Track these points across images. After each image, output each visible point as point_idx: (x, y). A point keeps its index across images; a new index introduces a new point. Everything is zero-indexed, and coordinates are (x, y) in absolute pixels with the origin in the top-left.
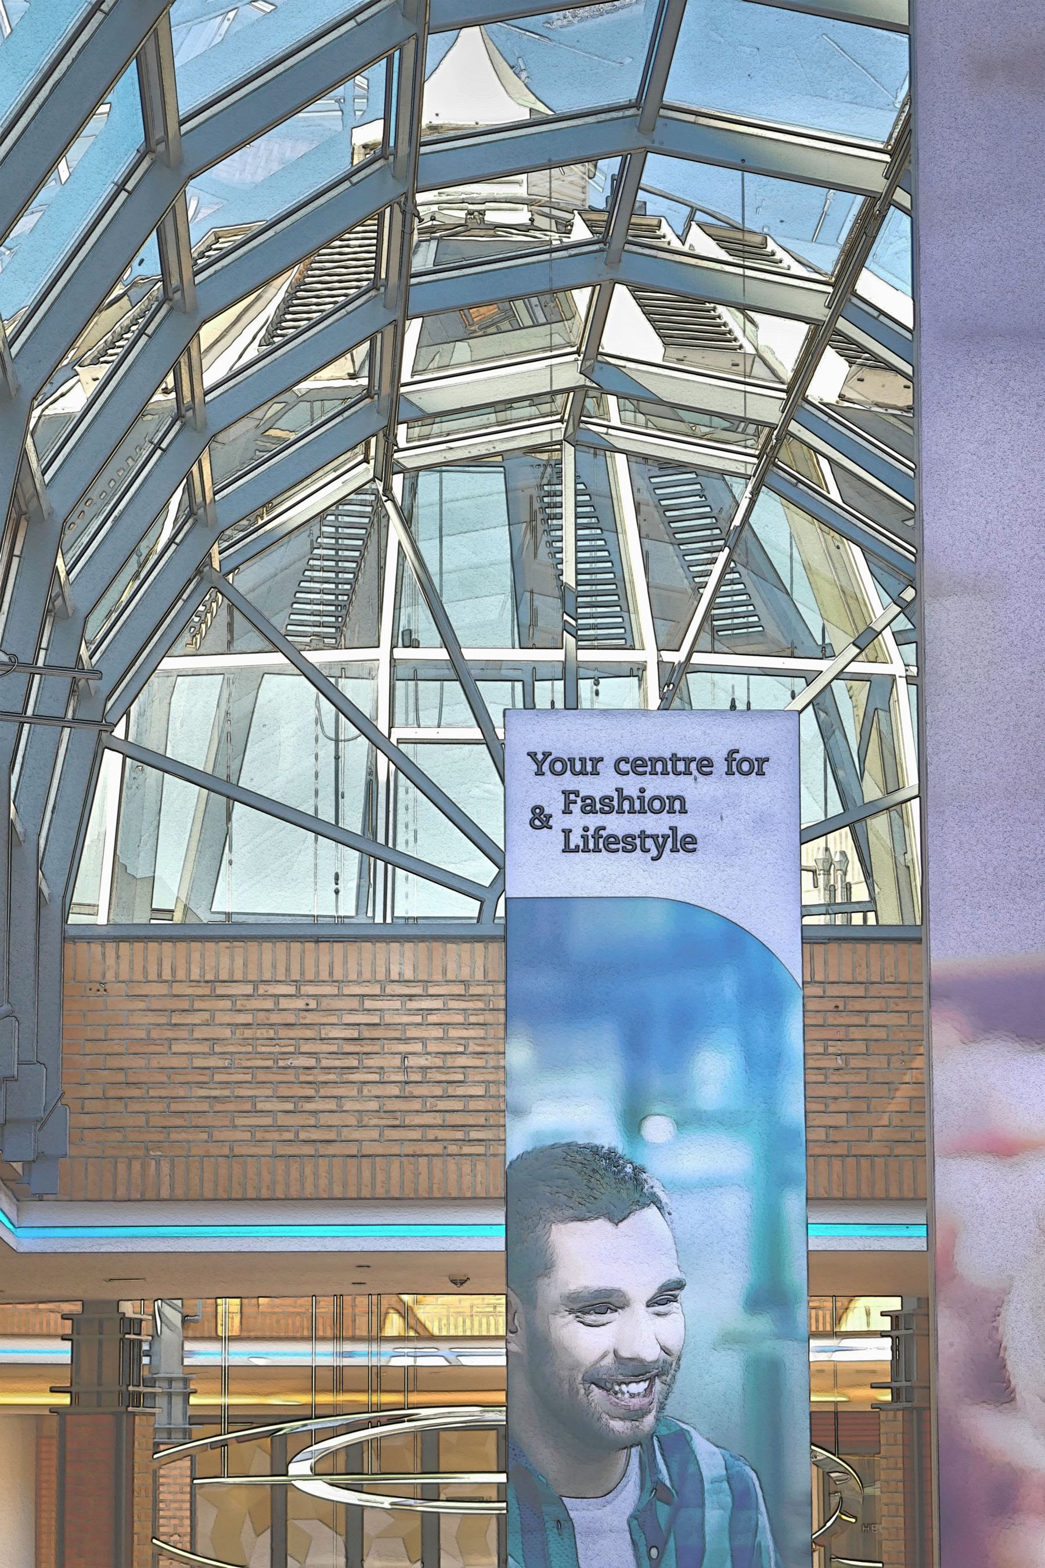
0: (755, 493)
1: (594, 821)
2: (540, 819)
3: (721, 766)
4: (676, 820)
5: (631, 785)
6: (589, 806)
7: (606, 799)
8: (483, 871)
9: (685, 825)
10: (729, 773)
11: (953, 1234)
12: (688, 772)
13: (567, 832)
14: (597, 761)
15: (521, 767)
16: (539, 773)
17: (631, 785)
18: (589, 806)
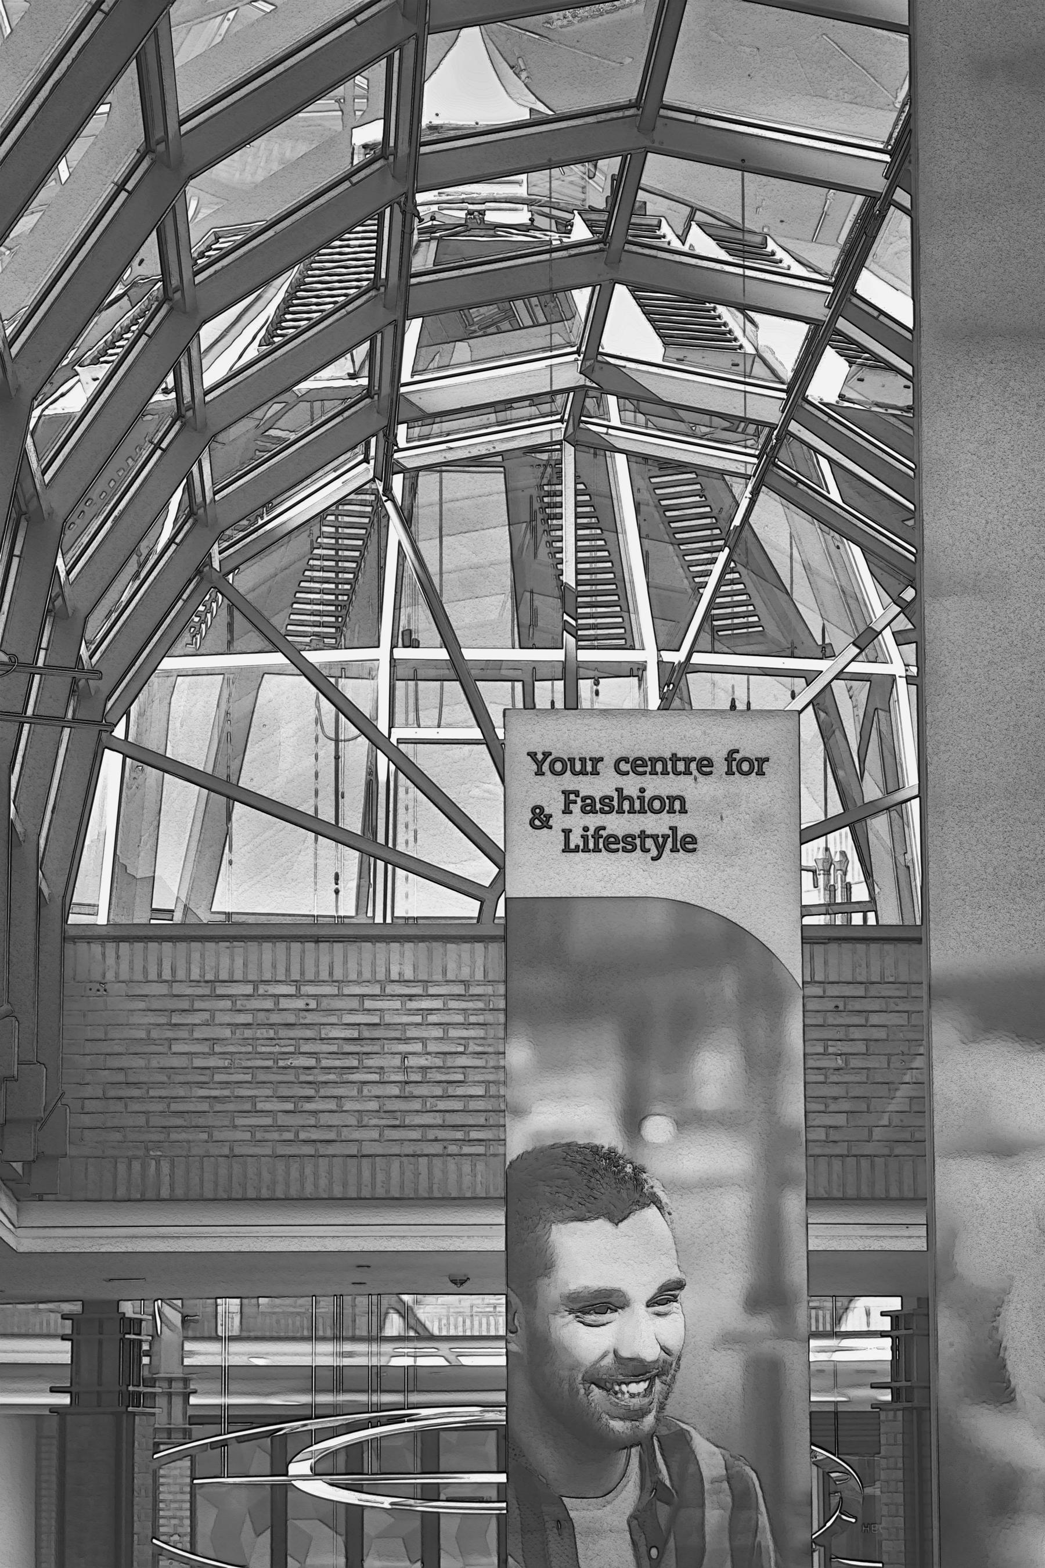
0: (755, 493)
1: (593, 821)
2: (540, 819)
3: (721, 766)
4: (676, 820)
5: (631, 785)
6: (589, 806)
7: (606, 799)
8: (483, 871)
9: (685, 825)
10: (729, 772)
13: (567, 832)
14: (596, 761)
15: (521, 767)
16: (539, 773)
17: (631, 785)
18: (589, 806)
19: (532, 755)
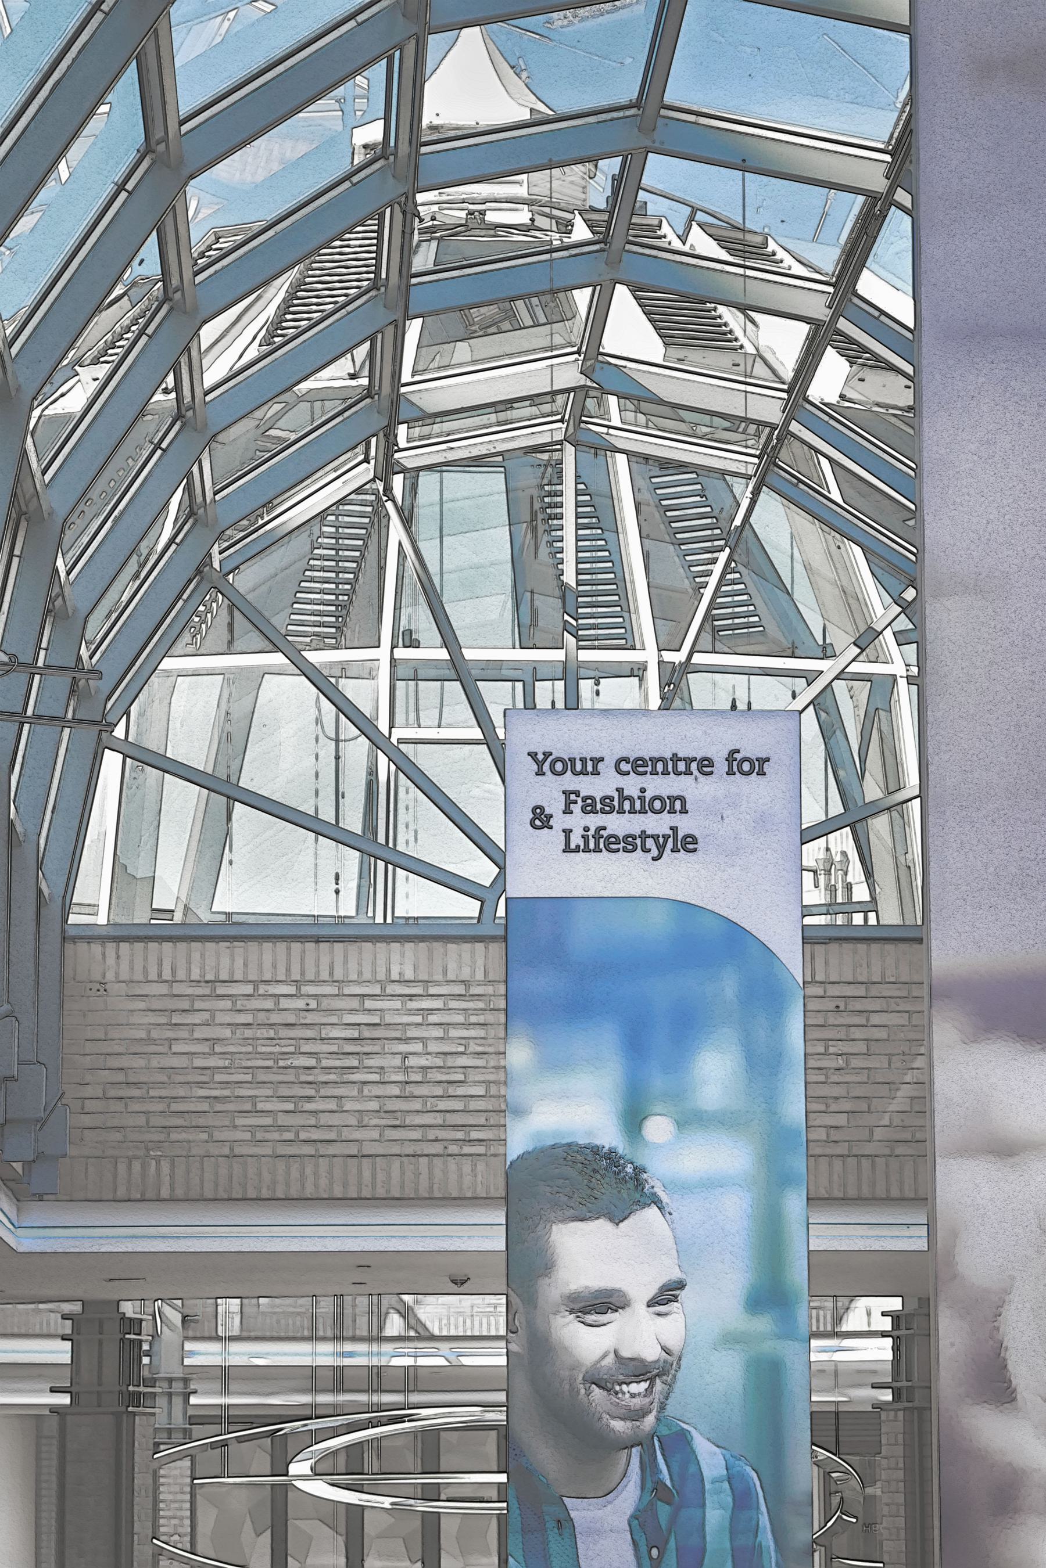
0: (756, 493)
1: (594, 821)
2: (541, 819)
3: (721, 766)
4: (677, 820)
5: (632, 785)
6: (590, 806)
7: (606, 800)
8: (483, 871)
9: (686, 825)
10: (730, 773)
11: (954, 1234)
12: (688, 772)
13: (567, 832)
14: (597, 761)
15: (521, 767)
16: (540, 773)
17: (632, 785)
18: (590, 806)
19: (533, 755)
